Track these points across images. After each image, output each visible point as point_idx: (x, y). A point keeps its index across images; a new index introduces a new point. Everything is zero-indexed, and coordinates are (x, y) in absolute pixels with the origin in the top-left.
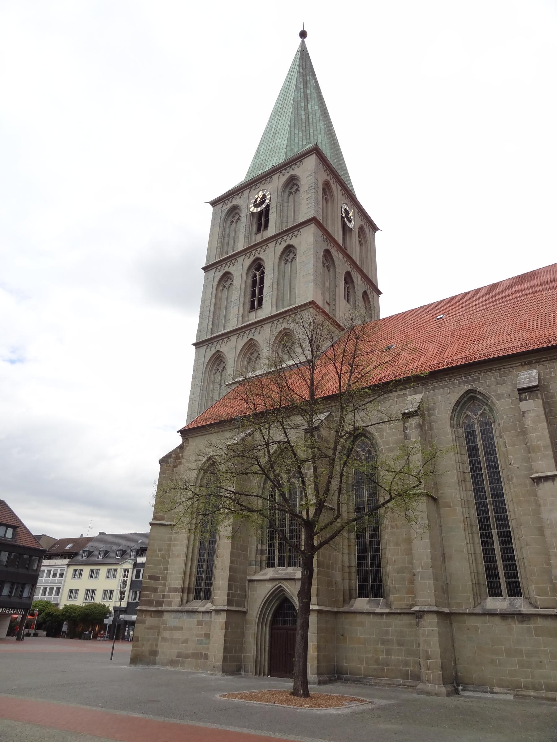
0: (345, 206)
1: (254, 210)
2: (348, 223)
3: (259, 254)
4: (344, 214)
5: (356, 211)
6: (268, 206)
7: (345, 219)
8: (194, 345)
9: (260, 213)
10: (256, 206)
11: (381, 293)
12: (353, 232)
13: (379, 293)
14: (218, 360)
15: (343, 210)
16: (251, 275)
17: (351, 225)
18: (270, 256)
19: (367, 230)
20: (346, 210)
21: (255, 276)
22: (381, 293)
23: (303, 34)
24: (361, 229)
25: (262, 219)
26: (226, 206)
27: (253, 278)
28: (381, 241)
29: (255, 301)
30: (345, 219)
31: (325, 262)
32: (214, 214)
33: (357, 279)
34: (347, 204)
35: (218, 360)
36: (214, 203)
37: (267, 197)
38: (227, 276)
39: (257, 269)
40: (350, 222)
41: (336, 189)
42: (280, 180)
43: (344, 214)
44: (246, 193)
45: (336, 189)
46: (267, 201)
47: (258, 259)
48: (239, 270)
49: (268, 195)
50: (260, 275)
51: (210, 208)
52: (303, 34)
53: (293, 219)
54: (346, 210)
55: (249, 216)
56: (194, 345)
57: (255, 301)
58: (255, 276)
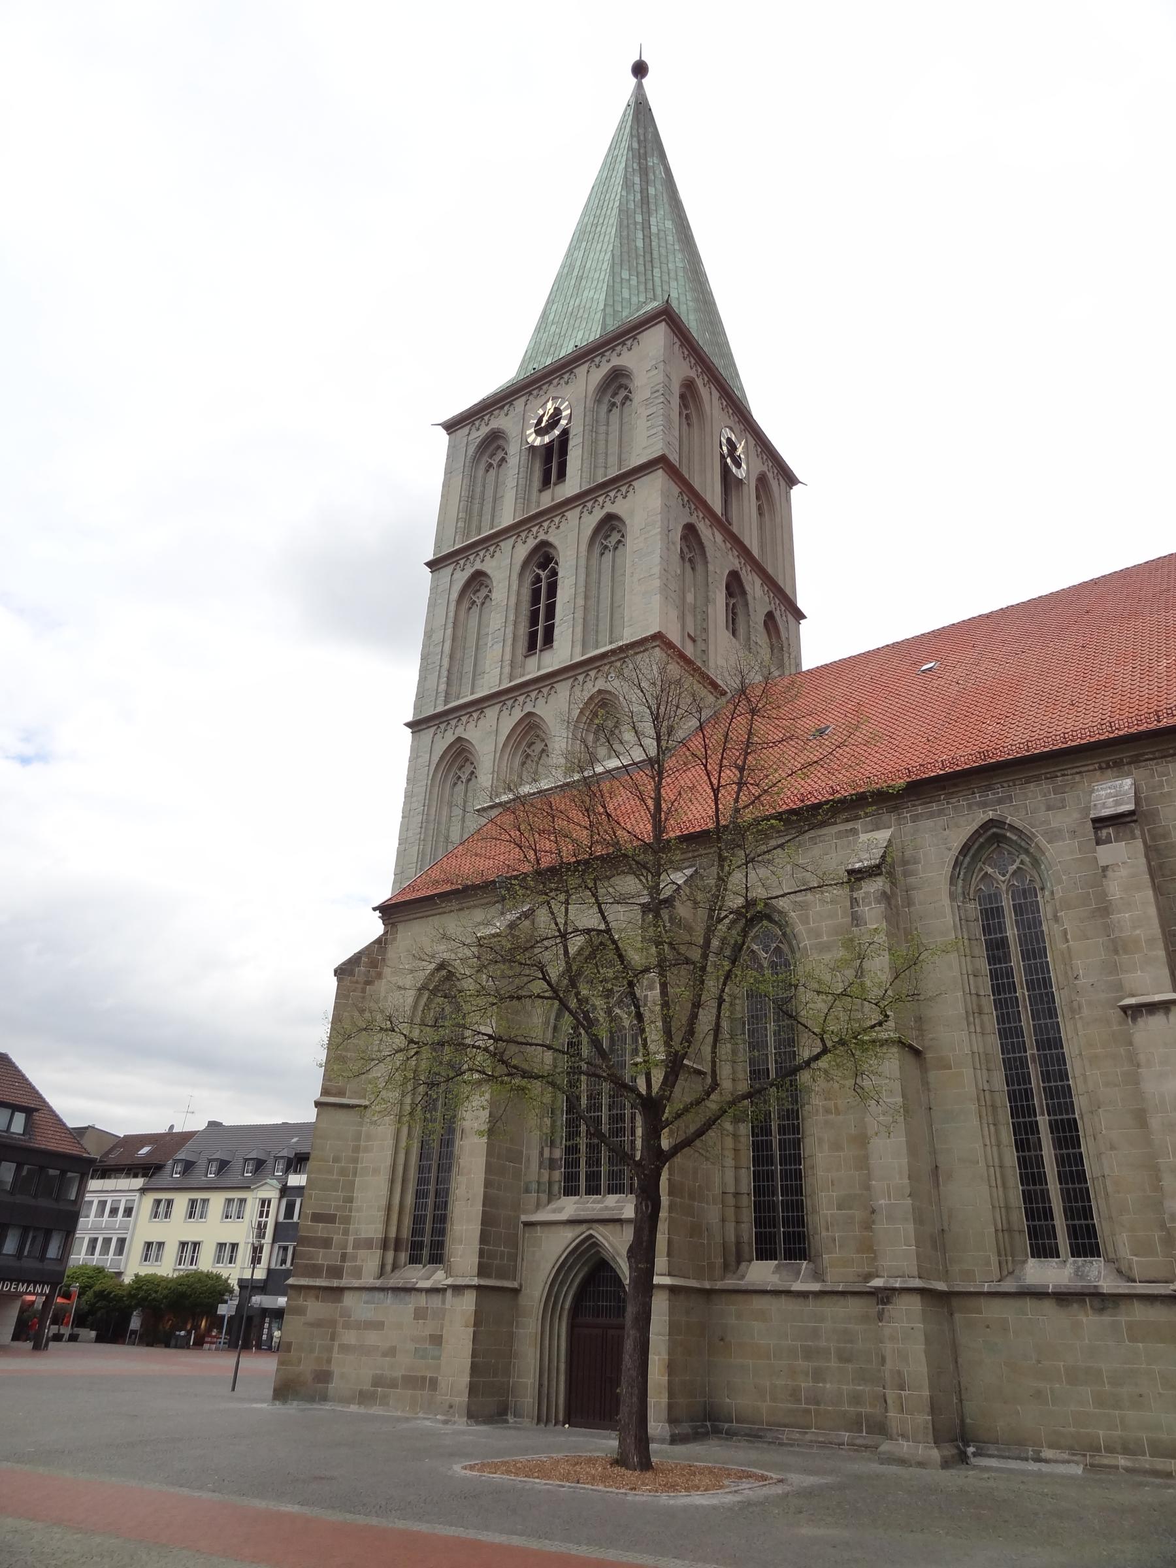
0: (727, 433)
1: (534, 440)
2: (734, 469)
3: (547, 533)
4: (725, 448)
5: (752, 442)
6: (565, 432)
7: (729, 460)
8: (409, 725)
9: (549, 448)
10: (540, 432)
11: (804, 617)
12: (745, 488)
13: (799, 615)
14: (459, 757)
15: (724, 441)
16: (529, 578)
17: (741, 473)
18: (570, 539)
19: (774, 484)
20: (729, 440)
21: (538, 579)
22: (804, 617)
23: (640, 69)
24: (762, 480)
25: (552, 460)
26: (478, 432)
27: (534, 583)
28: (804, 507)
29: (539, 632)
30: (729, 460)
31: (686, 550)
32: (415, 750)
33: (753, 585)
34: (731, 429)
35: (459, 757)
36: (451, 426)
37: (564, 414)
38: (478, 579)
39: (543, 566)
40: (739, 466)
41: (709, 396)
42: (589, 378)
43: (725, 448)
44: (519, 404)
45: (709, 396)
46: (563, 422)
47: (544, 544)
48: (504, 568)
49: (565, 409)
50: (548, 577)
51: (443, 437)
52: (640, 69)
53: (617, 459)
54: (729, 440)
55: (525, 453)
56: (409, 725)
57: (539, 632)
58: (538, 579)
